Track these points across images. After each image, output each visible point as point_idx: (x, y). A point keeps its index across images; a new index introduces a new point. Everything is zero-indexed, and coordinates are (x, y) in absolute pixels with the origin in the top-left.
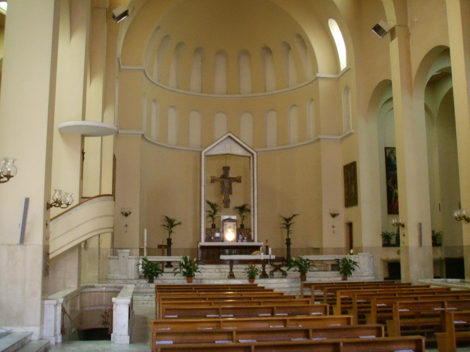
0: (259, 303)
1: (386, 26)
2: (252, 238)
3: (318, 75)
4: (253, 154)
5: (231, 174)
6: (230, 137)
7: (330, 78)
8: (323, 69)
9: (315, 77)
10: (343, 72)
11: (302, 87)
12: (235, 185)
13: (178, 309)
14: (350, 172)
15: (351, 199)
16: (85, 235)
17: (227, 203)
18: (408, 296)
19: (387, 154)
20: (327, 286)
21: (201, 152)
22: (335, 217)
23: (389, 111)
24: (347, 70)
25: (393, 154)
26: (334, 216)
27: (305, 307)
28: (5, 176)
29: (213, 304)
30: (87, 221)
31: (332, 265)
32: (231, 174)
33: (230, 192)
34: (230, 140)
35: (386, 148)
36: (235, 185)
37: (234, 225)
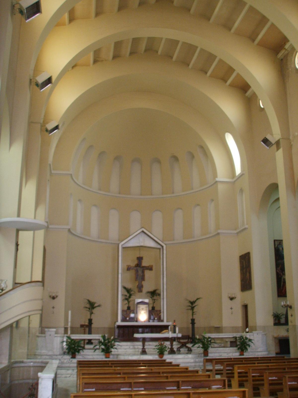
0: (167, 377)
1: (272, 139)
2: (162, 319)
3: (217, 179)
6: (143, 232)
7: (227, 182)
8: (222, 174)
14: (245, 261)
15: (246, 284)
19: (276, 246)
24: (241, 175)
29: (126, 378)
31: (231, 342)
33: (143, 279)
34: (143, 234)
37: (146, 307)
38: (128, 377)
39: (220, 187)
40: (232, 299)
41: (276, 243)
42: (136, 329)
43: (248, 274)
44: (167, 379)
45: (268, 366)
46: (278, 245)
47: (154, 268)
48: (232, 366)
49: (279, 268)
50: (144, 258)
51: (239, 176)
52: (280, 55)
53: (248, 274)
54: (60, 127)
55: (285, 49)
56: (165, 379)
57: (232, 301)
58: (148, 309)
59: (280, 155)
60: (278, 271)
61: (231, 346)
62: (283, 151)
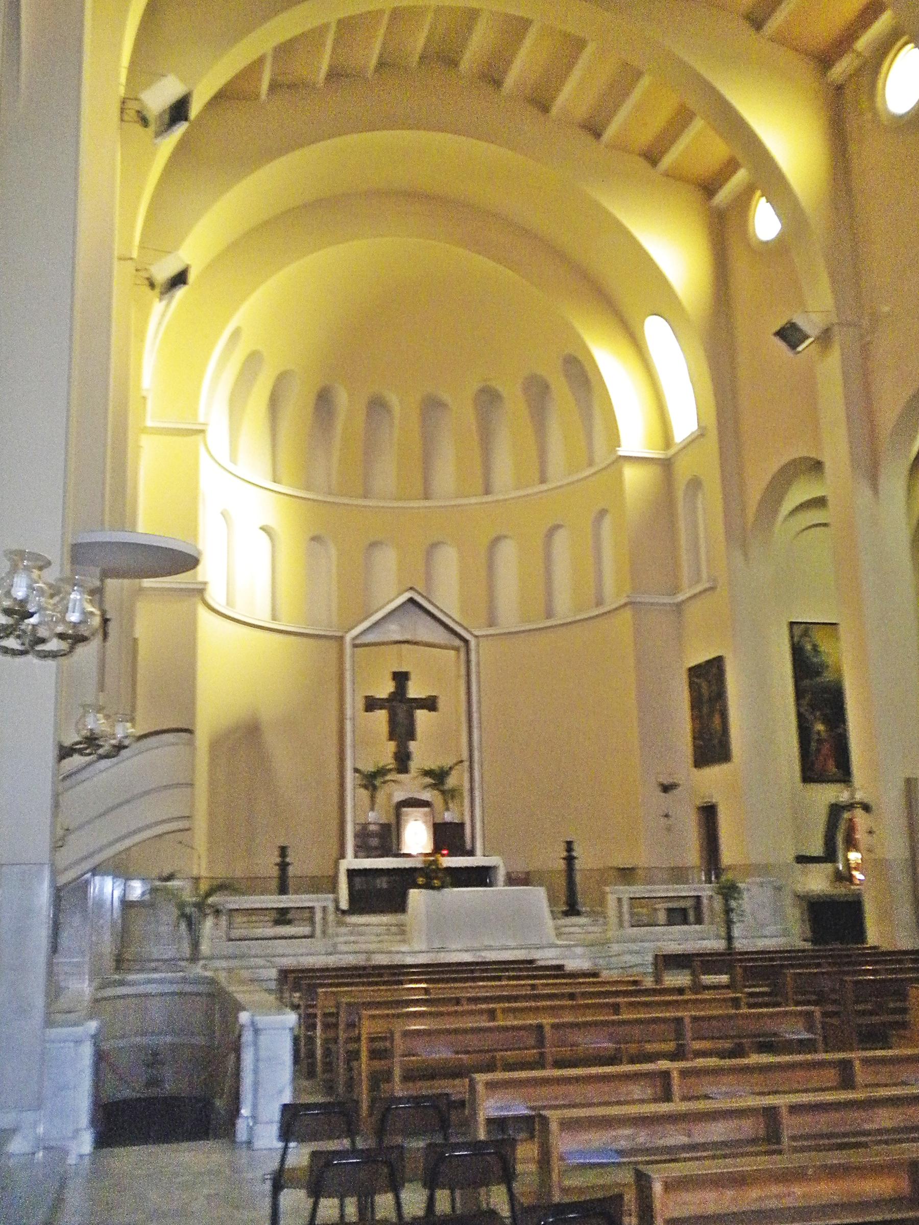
0: (616, 1008)
1: (810, 324)
2: (468, 846)
3: (622, 451)
4: (466, 642)
5: (414, 691)
6: (411, 600)
7: (652, 459)
8: (635, 437)
9: (613, 457)
10: (681, 446)
11: (578, 481)
12: (421, 715)
13: (449, 1032)
14: (708, 681)
15: (711, 747)
16: (157, 824)
17: (403, 760)
18: (592, 990)
19: (796, 639)
20: (792, 966)
21: (341, 638)
22: (670, 793)
23: (807, 529)
24: (693, 441)
25: (808, 639)
26: (666, 788)
27: (730, 1017)
28: (62, 636)
29: (499, 1014)
30: (166, 787)
31: (670, 911)
32: (414, 691)
33: (411, 735)
34: (412, 608)
35: (792, 624)
36: (421, 715)
37: (425, 815)
38: (504, 1010)
39: (632, 476)
40: (666, 788)
41: (797, 631)
42: (406, 879)
43: (717, 720)
44: (738, 1007)
45: (533, 987)
46: (801, 637)
47: (441, 704)
48: (311, 990)
49: (804, 702)
50: (413, 676)
51: (684, 444)
52: (841, 68)
53: (717, 720)
54: (192, 277)
55: (854, 51)
56: (607, 1014)
57: (667, 795)
58: (430, 819)
59: (830, 369)
60: (802, 710)
61: (670, 923)
62: (845, 359)
